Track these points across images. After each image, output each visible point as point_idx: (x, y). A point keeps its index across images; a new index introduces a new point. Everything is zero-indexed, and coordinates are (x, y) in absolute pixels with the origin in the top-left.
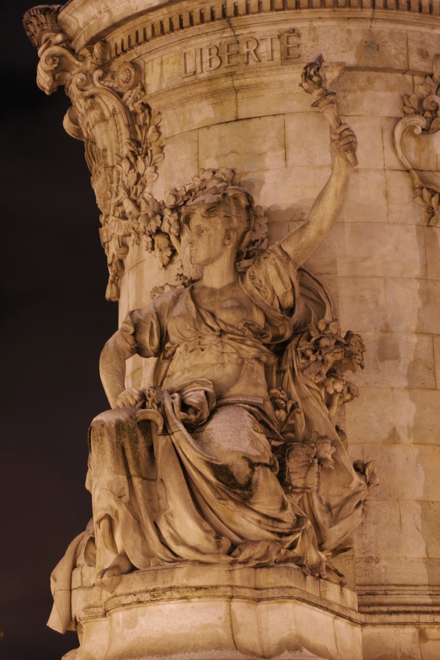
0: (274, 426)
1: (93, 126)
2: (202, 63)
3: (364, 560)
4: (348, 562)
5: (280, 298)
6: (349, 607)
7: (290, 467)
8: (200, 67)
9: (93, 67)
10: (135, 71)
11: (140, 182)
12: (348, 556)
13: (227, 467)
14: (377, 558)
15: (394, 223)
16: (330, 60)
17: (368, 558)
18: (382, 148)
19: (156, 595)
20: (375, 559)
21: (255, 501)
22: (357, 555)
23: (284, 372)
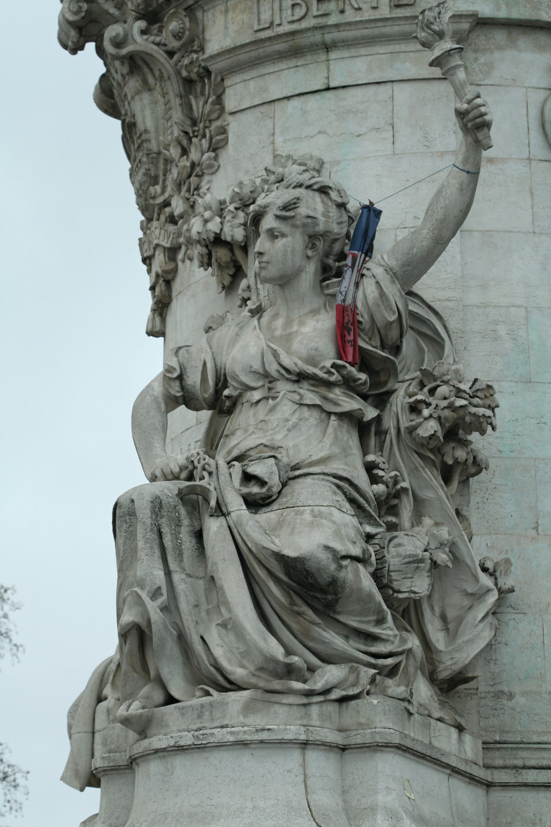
0: (371, 507)
1: (133, 98)
2: (281, 10)
3: (492, 695)
4: (470, 698)
5: (382, 331)
6: (470, 760)
7: (392, 563)
8: (278, 16)
9: (133, 17)
10: (190, 21)
11: (194, 174)
12: (470, 689)
13: (303, 561)
14: (511, 694)
15: (541, 233)
16: (458, 8)
17: (498, 692)
18: (527, 130)
19: (201, 737)
20: (508, 694)
21: (341, 609)
22: (483, 688)
23: (386, 432)
